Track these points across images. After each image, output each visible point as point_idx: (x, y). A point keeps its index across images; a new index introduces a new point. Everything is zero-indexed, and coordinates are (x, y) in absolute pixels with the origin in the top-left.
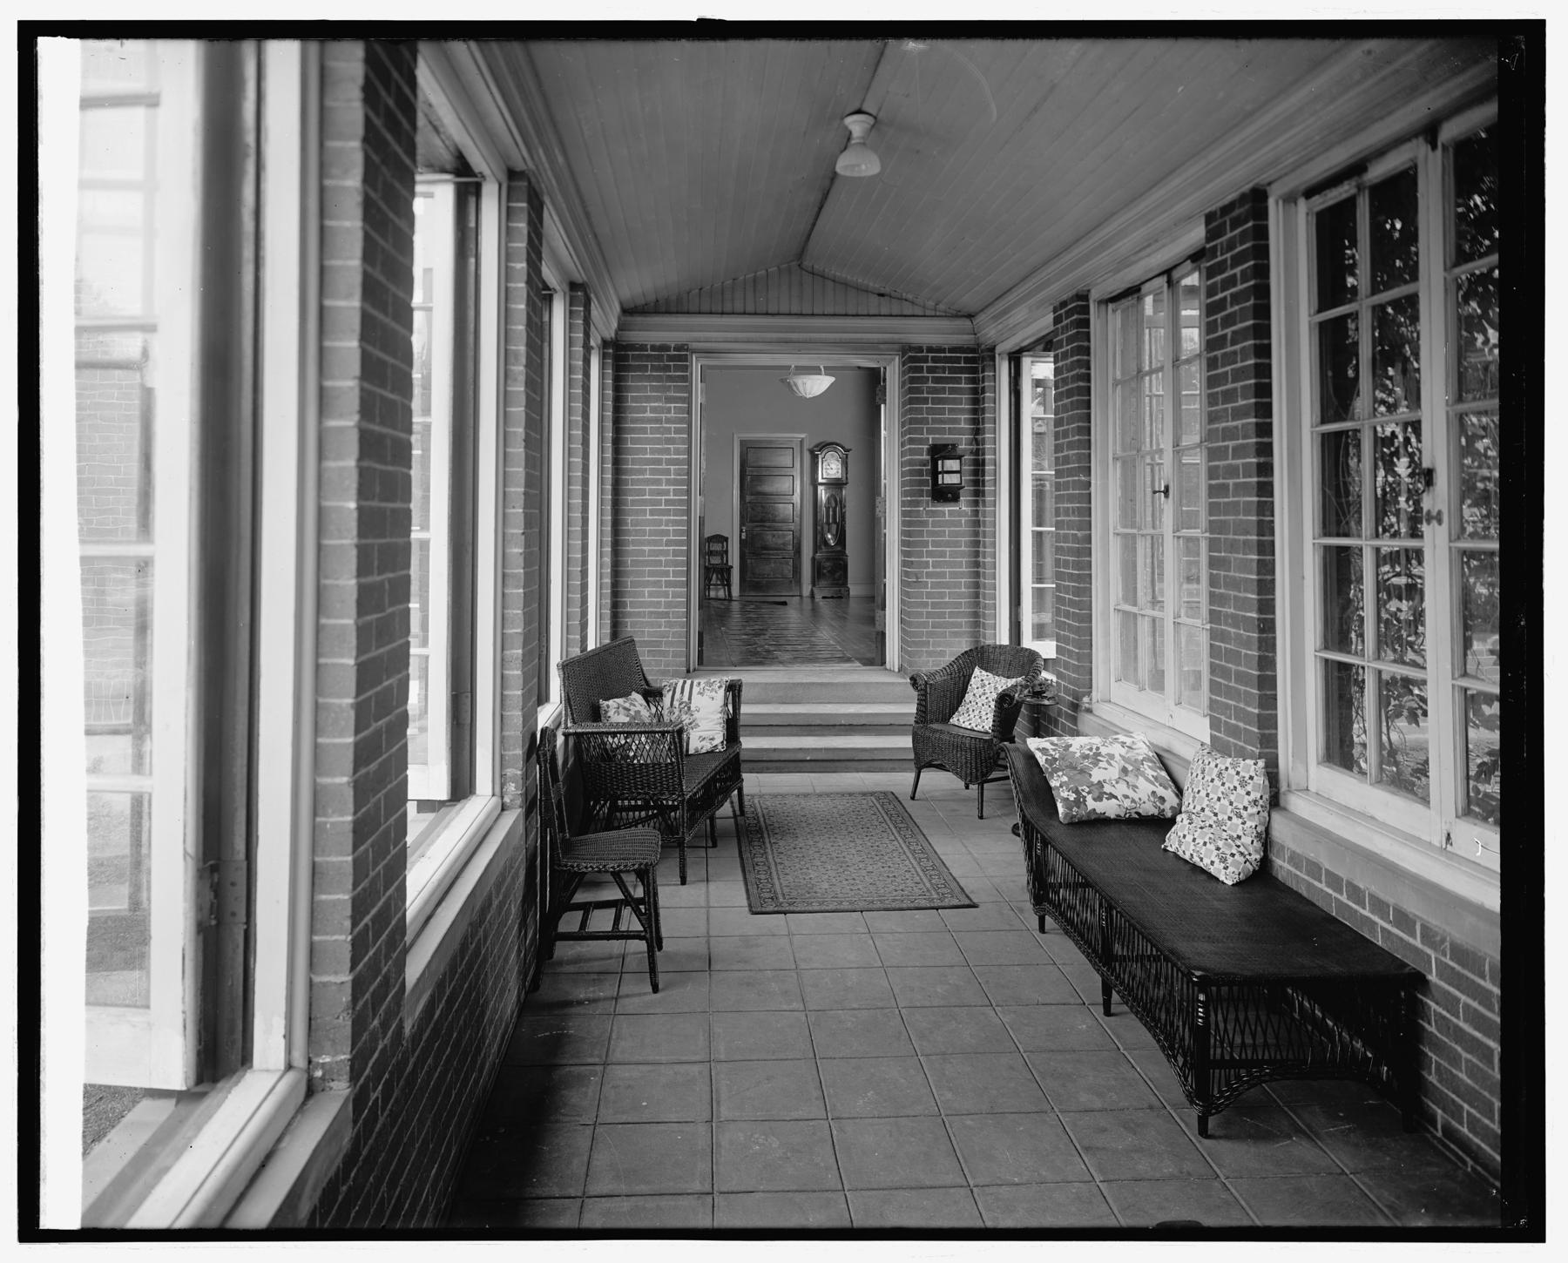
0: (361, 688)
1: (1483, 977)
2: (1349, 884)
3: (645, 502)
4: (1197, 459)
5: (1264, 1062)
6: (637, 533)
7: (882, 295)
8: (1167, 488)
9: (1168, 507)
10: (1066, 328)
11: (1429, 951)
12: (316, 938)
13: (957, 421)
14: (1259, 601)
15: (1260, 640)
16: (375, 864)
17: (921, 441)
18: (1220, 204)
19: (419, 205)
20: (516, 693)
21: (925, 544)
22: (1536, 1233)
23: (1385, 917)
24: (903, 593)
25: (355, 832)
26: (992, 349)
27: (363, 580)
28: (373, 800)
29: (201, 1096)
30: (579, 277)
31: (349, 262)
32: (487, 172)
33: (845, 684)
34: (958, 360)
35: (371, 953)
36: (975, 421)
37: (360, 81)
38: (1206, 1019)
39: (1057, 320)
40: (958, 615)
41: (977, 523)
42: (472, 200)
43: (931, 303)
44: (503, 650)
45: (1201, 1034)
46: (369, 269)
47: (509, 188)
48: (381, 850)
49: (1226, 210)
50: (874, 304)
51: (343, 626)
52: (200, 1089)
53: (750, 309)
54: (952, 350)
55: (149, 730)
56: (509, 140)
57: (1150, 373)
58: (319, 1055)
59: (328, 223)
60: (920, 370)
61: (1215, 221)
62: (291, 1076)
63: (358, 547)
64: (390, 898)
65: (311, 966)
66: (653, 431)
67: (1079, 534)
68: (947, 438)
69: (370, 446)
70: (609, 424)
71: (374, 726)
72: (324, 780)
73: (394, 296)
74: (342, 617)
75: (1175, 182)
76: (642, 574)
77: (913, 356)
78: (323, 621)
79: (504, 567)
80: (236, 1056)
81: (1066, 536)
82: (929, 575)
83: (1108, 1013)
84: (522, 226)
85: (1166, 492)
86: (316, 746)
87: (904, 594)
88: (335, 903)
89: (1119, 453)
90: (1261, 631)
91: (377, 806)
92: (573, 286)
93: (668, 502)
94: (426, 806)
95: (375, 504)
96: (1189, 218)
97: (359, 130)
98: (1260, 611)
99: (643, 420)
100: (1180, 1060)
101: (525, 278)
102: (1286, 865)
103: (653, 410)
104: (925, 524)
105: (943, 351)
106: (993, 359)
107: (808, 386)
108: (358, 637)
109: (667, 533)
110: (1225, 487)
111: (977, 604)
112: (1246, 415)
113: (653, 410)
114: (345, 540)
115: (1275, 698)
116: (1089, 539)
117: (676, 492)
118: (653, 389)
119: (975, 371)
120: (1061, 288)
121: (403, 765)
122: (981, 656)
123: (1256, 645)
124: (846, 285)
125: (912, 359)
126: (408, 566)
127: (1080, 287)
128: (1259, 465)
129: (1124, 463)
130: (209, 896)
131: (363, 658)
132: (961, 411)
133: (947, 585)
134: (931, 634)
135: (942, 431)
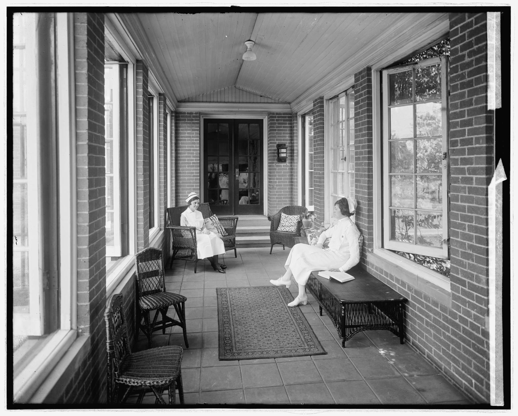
1: (422, 298)
2: (390, 274)
3: (185, 163)
5: (361, 325)
7: (261, 96)
8: (345, 158)
10: (317, 108)
11: (409, 292)
13: (285, 137)
14: (368, 192)
15: (368, 204)
16: (96, 272)
17: (274, 143)
18: (359, 71)
19: (106, 70)
20: (141, 223)
21: (276, 176)
23: (399, 283)
25: (89, 262)
26: (297, 114)
27: (91, 189)
28: (95, 253)
30: (162, 92)
32: (129, 61)
33: (250, 220)
34: (285, 117)
35: (95, 297)
36: (291, 137)
37: (86, 41)
38: (344, 313)
39: (314, 105)
40: (286, 198)
41: (292, 169)
42: (125, 69)
43: (277, 99)
45: (343, 319)
46: (90, 97)
47: (137, 65)
49: (360, 73)
50: (259, 99)
51: (85, 203)
52: (45, 336)
53: (219, 100)
54: (284, 114)
55: (27, 235)
56: (135, 51)
58: (80, 326)
59: (77, 71)
60: (274, 120)
61: (358, 76)
62: (72, 331)
63: (88, 179)
64: (100, 282)
65: (77, 300)
66: (188, 140)
67: (321, 172)
69: (91, 149)
70: (174, 138)
71: (95, 232)
72: (80, 247)
73: (99, 104)
76: (185, 186)
77: (271, 116)
79: (137, 184)
80: (56, 326)
81: (317, 173)
82: (277, 185)
83: (321, 315)
84: (141, 77)
86: (77, 237)
87: (269, 192)
88: (84, 282)
90: (369, 201)
91: (96, 255)
93: (193, 163)
94: (114, 258)
95: (94, 166)
96: (350, 75)
98: (368, 195)
99: (185, 137)
102: (375, 270)
103: (188, 133)
104: (275, 169)
105: (281, 114)
108: (89, 206)
109: (193, 173)
110: (359, 158)
111: (292, 195)
112: (365, 136)
113: (188, 133)
114: (85, 177)
116: (323, 174)
117: (196, 160)
118: (188, 127)
119: (291, 120)
121: (104, 244)
122: (290, 210)
124: (250, 93)
126: (105, 185)
127: (321, 95)
128: (368, 151)
129: (334, 150)
130: (46, 281)
132: (287, 133)
133: (283, 189)
135: (281, 140)
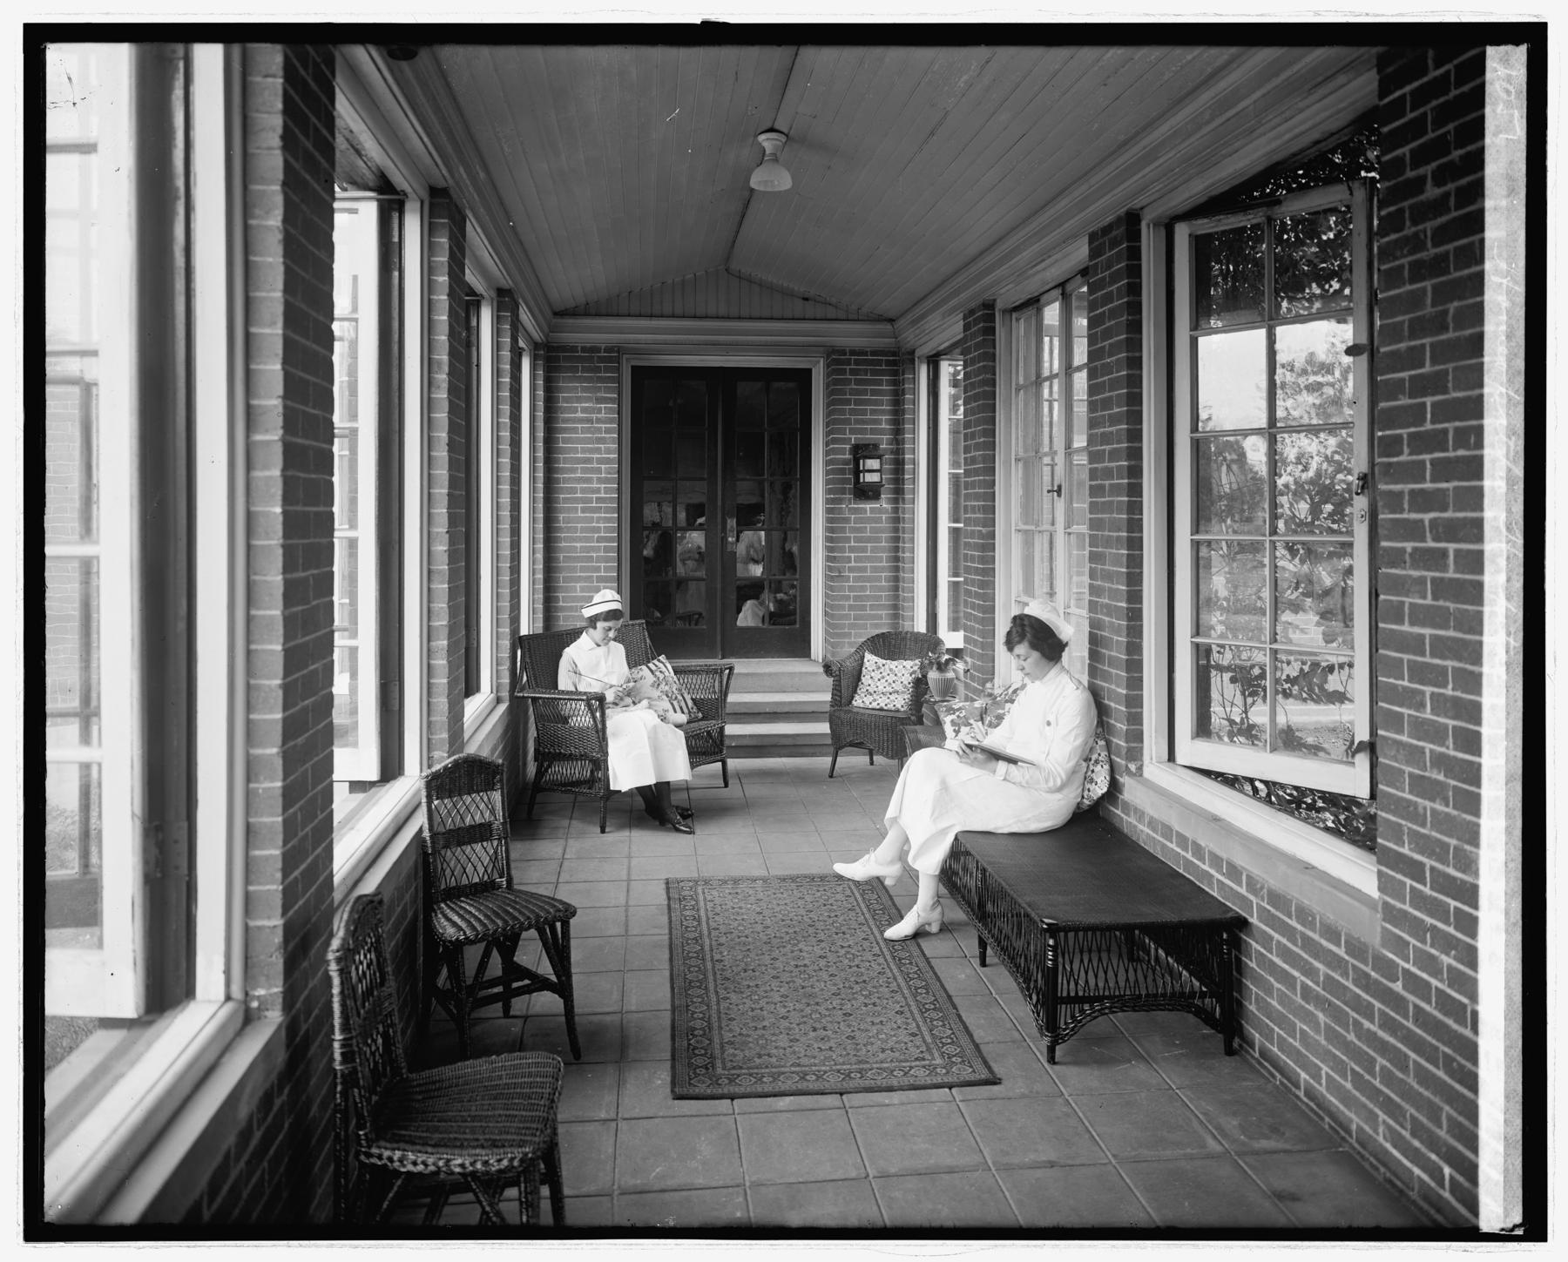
0: (288, 670)
2: (1194, 843)
3: (576, 500)
4: (1082, 460)
6: (569, 530)
7: (806, 299)
8: (1060, 487)
9: (1060, 505)
10: (974, 336)
11: (1251, 897)
12: (251, 888)
13: (878, 422)
14: (1128, 592)
15: (1128, 627)
20: (441, 681)
21: (848, 540)
22: (1544, 1238)
23: (1219, 870)
24: (827, 587)
25: (284, 795)
26: (912, 352)
27: (1478, 329)
29: (150, 1023)
30: (507, 282)
31: (272, 294)
32: (409, 190)
33: (770, 675)
37: (280, 131)
38: (1055, 960)
39: (966, 327)
41: (897, 520)
42: (396, 215)
44: (429, 641)
45: (1051, 975)
47: (432, 205)
48: (309, 814)
49: (1106, 230)
52: (149, 1018)
54: (874, 353)
56: (428, 160)
57: (1047, 379)
60: (843, 372)
62: (230, 1006)
63: (283, 546)
67: (984, 530)
68: (870, 437)
70: (540, 424)
74: (269, 608)
75: (1063, 203)
76: (574, 569)
77: (837, 359)
78: (253, 612)
82: (851, 569)
83: (983, 964)
85: (1059, 491)
88: (267, 858)
89: (1021, 454)
90: (1129, 619)
92: (501, 292)
94: (357, 786)
96: (1073, 236)
97: (280, 175)
98: (1129, 601)
100: (1034, 997)
101: (447, 290)
102: (1146, 830)
104: (847, 520)
105: (865, 353)
106: (913, 361)
107: (1505, 61)
108: (285, 626)
109: (598, 530)
110: (1102, 487)
111: (897, 597)
113: (584, 410)
114: (272, 540)
115: (1141, 679)
116: (992, 535)
118: (585, 390)
119: (896, 373)
120: (970, 296)
123: (1124, 633)
125: (838, 362)
126: (332, 564)
127: (987, 296)
128: (1129, 467)
130: (155, 851)
131: (292, 644)
132: (883, 412)
133: (869, 579)
134: (852, 626)
135: (863, 431)
